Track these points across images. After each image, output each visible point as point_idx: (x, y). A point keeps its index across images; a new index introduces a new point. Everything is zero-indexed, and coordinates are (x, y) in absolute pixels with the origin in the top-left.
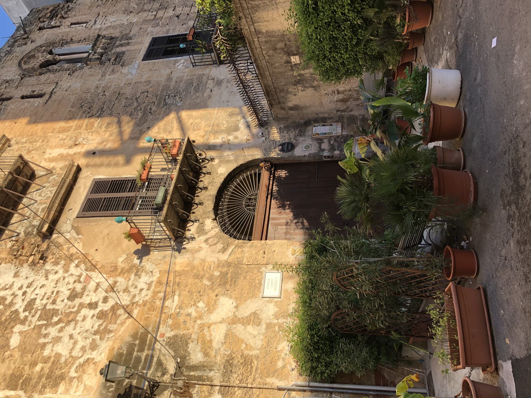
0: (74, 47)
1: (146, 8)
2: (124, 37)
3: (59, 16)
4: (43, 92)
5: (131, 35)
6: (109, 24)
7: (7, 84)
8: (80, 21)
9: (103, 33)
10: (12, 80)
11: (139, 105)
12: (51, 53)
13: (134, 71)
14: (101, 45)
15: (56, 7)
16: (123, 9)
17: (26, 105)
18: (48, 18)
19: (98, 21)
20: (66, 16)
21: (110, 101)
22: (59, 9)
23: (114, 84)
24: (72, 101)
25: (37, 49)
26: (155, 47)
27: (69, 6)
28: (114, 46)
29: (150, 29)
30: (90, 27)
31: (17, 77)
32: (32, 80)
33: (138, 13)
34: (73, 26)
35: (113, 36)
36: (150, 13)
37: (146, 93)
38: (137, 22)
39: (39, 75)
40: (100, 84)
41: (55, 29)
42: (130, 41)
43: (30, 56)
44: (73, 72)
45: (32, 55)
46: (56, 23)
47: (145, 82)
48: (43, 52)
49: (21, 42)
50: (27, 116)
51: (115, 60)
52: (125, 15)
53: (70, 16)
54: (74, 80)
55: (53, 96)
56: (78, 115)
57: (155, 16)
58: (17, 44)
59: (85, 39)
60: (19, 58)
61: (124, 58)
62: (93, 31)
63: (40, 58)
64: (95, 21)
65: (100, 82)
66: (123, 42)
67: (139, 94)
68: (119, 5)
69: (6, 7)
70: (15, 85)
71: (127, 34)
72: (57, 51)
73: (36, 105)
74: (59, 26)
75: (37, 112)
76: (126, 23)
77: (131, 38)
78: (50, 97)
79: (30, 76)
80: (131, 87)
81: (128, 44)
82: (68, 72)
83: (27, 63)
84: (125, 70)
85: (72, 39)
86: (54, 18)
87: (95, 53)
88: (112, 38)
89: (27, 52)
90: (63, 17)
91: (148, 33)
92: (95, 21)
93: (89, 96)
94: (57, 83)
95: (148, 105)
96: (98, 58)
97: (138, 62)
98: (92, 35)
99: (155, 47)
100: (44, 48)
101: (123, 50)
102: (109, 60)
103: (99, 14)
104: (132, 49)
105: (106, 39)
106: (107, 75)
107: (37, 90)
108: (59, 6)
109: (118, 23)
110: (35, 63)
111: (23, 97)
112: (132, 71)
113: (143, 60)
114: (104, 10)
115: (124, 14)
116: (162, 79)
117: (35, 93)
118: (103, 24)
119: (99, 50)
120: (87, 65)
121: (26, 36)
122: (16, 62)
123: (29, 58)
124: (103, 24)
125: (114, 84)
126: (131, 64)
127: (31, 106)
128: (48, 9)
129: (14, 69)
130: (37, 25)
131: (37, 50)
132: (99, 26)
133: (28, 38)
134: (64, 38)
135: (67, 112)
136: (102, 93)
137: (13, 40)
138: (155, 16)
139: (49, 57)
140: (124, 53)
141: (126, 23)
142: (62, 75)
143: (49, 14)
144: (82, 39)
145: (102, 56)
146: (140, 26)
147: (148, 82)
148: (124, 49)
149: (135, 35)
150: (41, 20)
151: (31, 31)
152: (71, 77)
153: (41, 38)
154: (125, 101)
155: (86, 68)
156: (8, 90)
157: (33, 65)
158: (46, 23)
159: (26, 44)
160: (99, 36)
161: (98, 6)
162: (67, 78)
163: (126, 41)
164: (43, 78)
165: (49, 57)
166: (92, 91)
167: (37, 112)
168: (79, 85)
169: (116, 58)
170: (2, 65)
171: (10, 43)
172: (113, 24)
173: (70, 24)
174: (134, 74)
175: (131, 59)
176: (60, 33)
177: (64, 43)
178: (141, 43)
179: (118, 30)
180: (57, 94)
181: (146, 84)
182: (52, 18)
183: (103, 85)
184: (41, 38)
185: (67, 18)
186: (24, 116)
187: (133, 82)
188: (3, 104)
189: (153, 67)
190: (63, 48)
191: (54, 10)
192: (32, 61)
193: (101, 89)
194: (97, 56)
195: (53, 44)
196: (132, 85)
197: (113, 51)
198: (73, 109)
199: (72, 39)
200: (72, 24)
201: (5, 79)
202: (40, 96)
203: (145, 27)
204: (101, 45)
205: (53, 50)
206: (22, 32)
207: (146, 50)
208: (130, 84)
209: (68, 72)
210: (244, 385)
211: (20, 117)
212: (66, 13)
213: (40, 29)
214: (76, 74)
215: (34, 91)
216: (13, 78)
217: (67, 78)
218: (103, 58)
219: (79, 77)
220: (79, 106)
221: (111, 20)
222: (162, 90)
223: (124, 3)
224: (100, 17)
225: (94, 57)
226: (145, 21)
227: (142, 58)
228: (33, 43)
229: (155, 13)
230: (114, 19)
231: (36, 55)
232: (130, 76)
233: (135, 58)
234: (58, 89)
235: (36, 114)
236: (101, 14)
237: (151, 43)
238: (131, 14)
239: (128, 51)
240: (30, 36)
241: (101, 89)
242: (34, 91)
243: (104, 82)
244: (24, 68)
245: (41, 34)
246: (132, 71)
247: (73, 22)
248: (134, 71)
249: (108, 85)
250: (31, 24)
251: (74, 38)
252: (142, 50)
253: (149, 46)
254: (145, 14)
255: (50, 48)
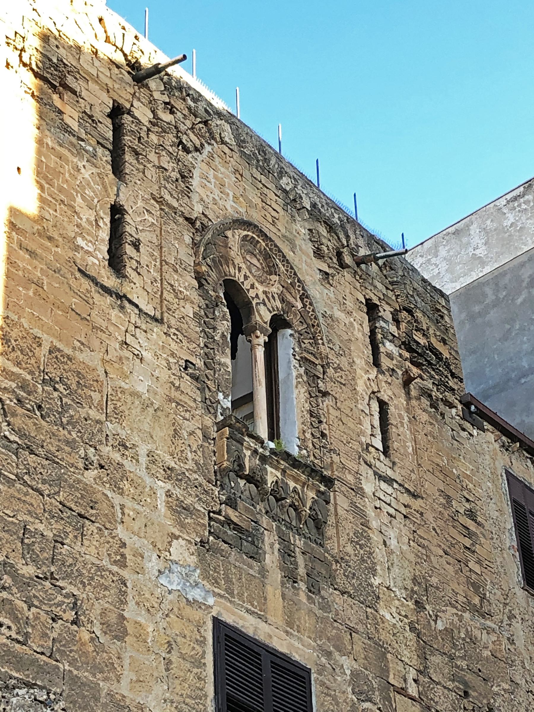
0: (295, 398)
1: (436, 659)
2: (319, 567)
3: (415, 371)
4: (129, 271)
5: (328, 592)
6: (374, 524)
7: (175, 175)
8: (393, 430)
9: (341, 501)
10: (187, 192)
11: (24, 584)
12: (279, 323)
13: (173, 582)
14: (292, 484)
15: (447, 366)
16: (434, 580)
17: (87, 215)
18: (409, 335)
19: (390, 490)
20: (414, 393)
21: (58, 482)
22: (441, 374)
23: (129, 503)
24: (80, 357)
25: (295, 283)
26: (267, 674)
27: (451, 406)
28: (290, 527)
29: (347, 663)
30: (369, 458)
31: (198, 209)
32: (181, 247)
33: (412, 629)
34: (375, 406)
35: (330, 531)
36: (412, 674)
37: (70, 615)
38: (378, 622)
39: (196, 272)
40: (135, 458)
41: (369, 351)
42: (303, 586)
43: (271, 259)
44: (196, 378)
45: (275, 266)
46: (390, 356)
47: (122, 618)
48: (283, 301)
49: (328, 244)
50: (41, 208)
51: (229, 522)
52: (409, 584)
53: (414, 402)
54: (164, 375)
55: (109, 299)
56: (18, 364)
57: (402, 691)
58: (323, 230)
59: (323, 435)
60: (267, 228)
61: (234, 554)
62: (351, 465)
63: (260, 288)
64: (389, 481)
65: (143, 460)
66: (300, 560)
67: (71, 589)
68: (450, 568)
69: (468, 226)
70: (167, 197)
71: (331, 578)
72: (287, 343)
73: (80, 241)
74: (376, 363)
75: (50, 239)
76: (376, 581)
77: (313, 589)
78: (107, 291)
79: (195, 245)
80: (105, 562)
81: (291, 577)
82: (199, 363)
83: (250, 247)
84: (181, 551)
85: (325, 394)
86: (407, 355)
87: (263, 459)
88: (319, 525)
89: (290, 255)
90: (407, 382)
91: (329, 654)
92: (389, 481)
93: (93, 413)
94: (159, 321)
95: (16, 619)
96: (241, 467)
97: (211, 601)
98: (336, 458)
99: (267, 674)
100: (299, 305)
101: (268, 558)
102: (231, 503)
103: (415, 496)
104: (269, 589)
105: (315, 502)
106: (168, 486)
107: (141, 257)
108: (453, 375)
109: (380, 554)
110: (244, 270)
111: (117, 212)
112: (175, 578)
113: (216, 621)
114: (429, 516)
115: (414, 580)
116: (124, 682)
117: (129, 250)
118: (378, 504)
119: (272, 475)
120: (220, 426)
121: (348, 260)
122: (256, 217)
123: (267, 257)
124: (378, 504)
125: (129, 503)
126: (205, 576)
127: (78, 226)
128: (444, 341)
129: (229, 204)
130: (385, 298)
131: (292, 284)
132: (368, 487)
133: (343, 265)
134: (330, 371)
135: (37, 332)
136: (95, 459)
137: (336, 220)
138: (402, 691)
139: (263, 315)
140: (256, 556)
141: (376, 581)
142: (190, 340)
143: (422, 341)
144: (323, 426)
145: (250, 479)
146: (360, 628)
147: (119, 631)
148: (271, 559)
149: (326, 607)
150: (404, 314)
151: (365, 279)
152: (175, 369)
153: (339, 305)
154: (49, 534)
155: (209, 421)
156: (151, 172)
157: (238, 260)
158: (393, 329)
159: (318, 254)
160: (329, 482)
161: (448, 498)
162: (173, 355)
163: (302, 571)
164: (186, 283)
165: (263, 315)
166: (111, 427)
167: (50, 239)
168: (142, 388)
169: (236, 527)
170: (246, 174)
171: (327, 212)
172: (376, 538)
173: (386, 398)
174: (163, 580)
175: (228, 580)
176: (352, 364)
177: (314, 370)
178: (290, 624)
179: (349, 549)
180: (114, 314)
181: (113, 618)
182: (410, 349)
183: (128, 465)
184: (339, 305)
185: (408, 393)
186: (42, 199)
187: (125, 573)
188: (100, 151)
189: (183, 657)
190: (294, 362)
191: (441, 359)
192: (255, 261)
193: (116, 456)
194: (249, 463)
195: (311, 332)
196: (115, 569)
197: (265, 521)
198: (43, 352)
199: (325, 394)
200: (383, 405)
201: (196, 173)
202: (116, 261)
203: (358, 647)
204: (292, 484)
205: (290, 331)
206: (363, 252)
207: (261, 637)
208: (122, 563)
209: (199, 363)
210: (163, 233)
211: (42, 188)
212: (425, 393)
213: (371, 309)
214: (187, 383)
215: (136, 245)
216: (195, 198)
217: (173, 355)
218: (242, 482)
219: (175, 394)
220: (55, 374)
221: (392, 533)
222: (74, 680)
223: (455, 586)
224: (406, 498)
225: (248, 453)
226: (380, 653)
227: (228, 618)
228: (319, 276)
229: (413, 690)
230: (393, 543)
231: (274, 278)
232: (153, 564)
233: (232, 594)
234: (134, 318)
235: (44, 234)
236: (417, 504)
237: (286, 658)
238: (411, 604)
239: (263, 572)
240: (347, 275)
241: (116, 456)
242: (136, 245)
243: (142, 472)
244: (229, 233)
245: (350, 304)
246: (175, 578)
247: (392, 410)
248: (173, 582)
249: (126, 485)
250: (392, 283)
251: (328, 401)
252: (262, 625)
253: (273, 653)
254: (409, 655)
255: (296, 322)
